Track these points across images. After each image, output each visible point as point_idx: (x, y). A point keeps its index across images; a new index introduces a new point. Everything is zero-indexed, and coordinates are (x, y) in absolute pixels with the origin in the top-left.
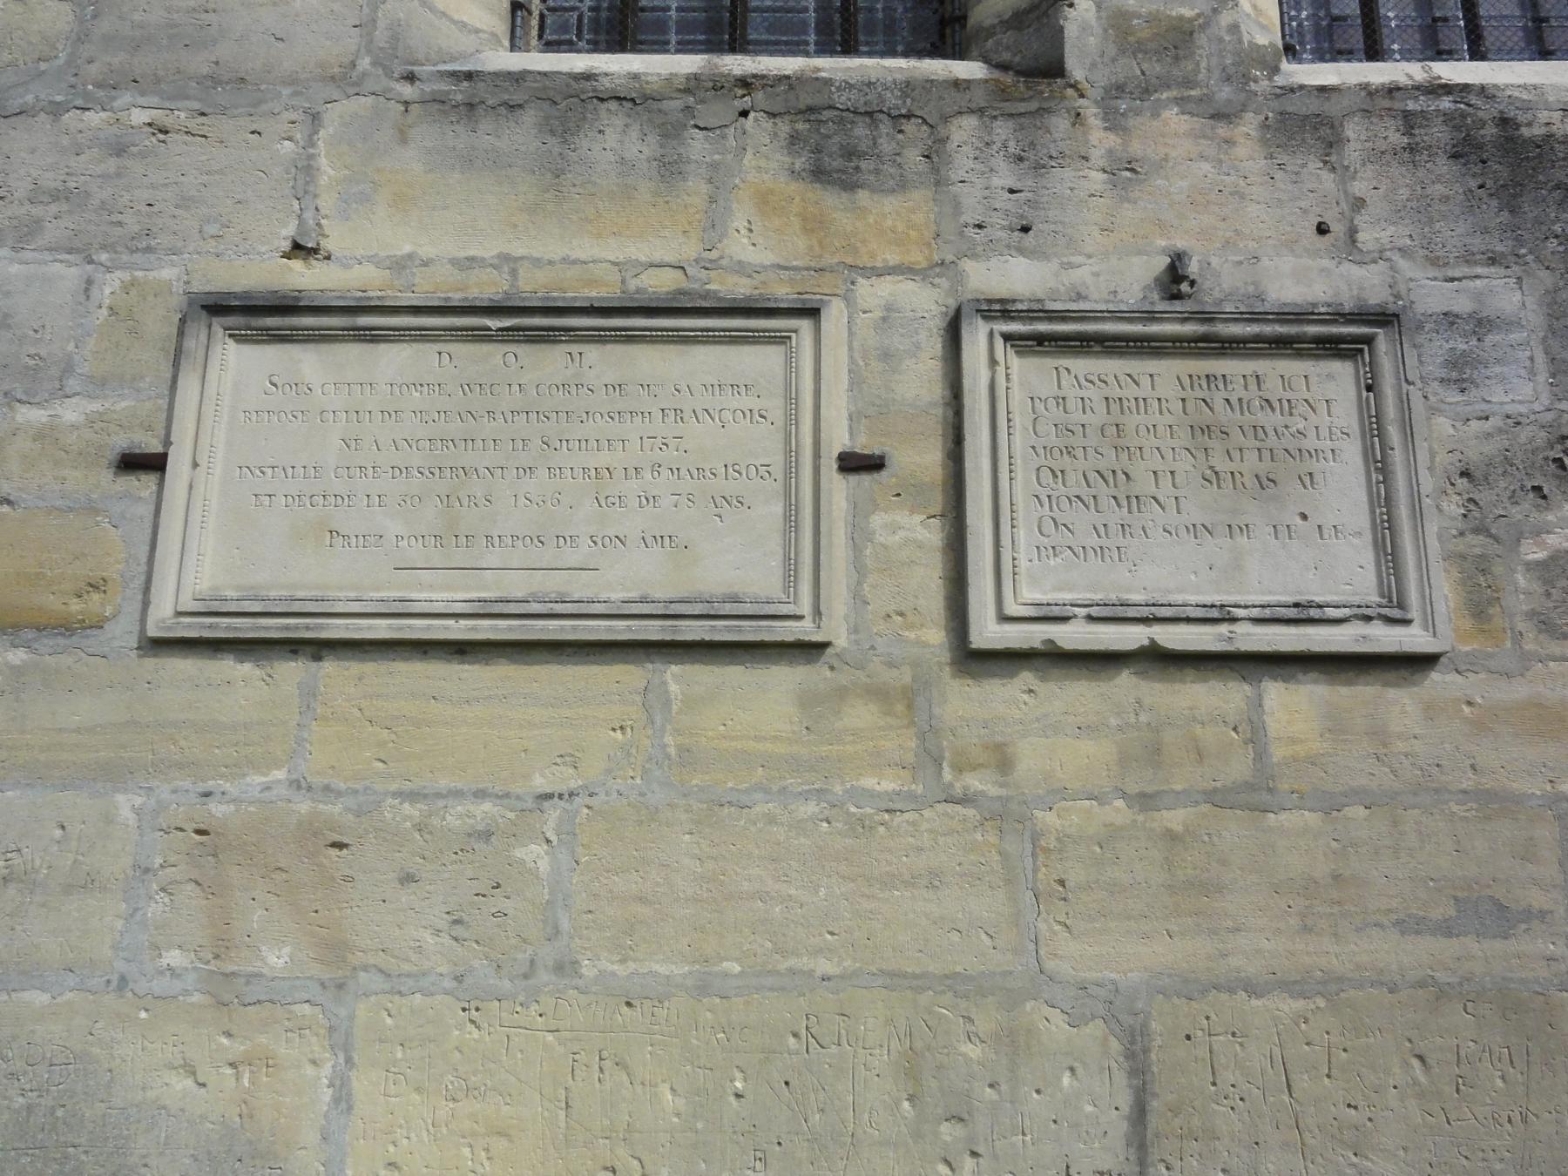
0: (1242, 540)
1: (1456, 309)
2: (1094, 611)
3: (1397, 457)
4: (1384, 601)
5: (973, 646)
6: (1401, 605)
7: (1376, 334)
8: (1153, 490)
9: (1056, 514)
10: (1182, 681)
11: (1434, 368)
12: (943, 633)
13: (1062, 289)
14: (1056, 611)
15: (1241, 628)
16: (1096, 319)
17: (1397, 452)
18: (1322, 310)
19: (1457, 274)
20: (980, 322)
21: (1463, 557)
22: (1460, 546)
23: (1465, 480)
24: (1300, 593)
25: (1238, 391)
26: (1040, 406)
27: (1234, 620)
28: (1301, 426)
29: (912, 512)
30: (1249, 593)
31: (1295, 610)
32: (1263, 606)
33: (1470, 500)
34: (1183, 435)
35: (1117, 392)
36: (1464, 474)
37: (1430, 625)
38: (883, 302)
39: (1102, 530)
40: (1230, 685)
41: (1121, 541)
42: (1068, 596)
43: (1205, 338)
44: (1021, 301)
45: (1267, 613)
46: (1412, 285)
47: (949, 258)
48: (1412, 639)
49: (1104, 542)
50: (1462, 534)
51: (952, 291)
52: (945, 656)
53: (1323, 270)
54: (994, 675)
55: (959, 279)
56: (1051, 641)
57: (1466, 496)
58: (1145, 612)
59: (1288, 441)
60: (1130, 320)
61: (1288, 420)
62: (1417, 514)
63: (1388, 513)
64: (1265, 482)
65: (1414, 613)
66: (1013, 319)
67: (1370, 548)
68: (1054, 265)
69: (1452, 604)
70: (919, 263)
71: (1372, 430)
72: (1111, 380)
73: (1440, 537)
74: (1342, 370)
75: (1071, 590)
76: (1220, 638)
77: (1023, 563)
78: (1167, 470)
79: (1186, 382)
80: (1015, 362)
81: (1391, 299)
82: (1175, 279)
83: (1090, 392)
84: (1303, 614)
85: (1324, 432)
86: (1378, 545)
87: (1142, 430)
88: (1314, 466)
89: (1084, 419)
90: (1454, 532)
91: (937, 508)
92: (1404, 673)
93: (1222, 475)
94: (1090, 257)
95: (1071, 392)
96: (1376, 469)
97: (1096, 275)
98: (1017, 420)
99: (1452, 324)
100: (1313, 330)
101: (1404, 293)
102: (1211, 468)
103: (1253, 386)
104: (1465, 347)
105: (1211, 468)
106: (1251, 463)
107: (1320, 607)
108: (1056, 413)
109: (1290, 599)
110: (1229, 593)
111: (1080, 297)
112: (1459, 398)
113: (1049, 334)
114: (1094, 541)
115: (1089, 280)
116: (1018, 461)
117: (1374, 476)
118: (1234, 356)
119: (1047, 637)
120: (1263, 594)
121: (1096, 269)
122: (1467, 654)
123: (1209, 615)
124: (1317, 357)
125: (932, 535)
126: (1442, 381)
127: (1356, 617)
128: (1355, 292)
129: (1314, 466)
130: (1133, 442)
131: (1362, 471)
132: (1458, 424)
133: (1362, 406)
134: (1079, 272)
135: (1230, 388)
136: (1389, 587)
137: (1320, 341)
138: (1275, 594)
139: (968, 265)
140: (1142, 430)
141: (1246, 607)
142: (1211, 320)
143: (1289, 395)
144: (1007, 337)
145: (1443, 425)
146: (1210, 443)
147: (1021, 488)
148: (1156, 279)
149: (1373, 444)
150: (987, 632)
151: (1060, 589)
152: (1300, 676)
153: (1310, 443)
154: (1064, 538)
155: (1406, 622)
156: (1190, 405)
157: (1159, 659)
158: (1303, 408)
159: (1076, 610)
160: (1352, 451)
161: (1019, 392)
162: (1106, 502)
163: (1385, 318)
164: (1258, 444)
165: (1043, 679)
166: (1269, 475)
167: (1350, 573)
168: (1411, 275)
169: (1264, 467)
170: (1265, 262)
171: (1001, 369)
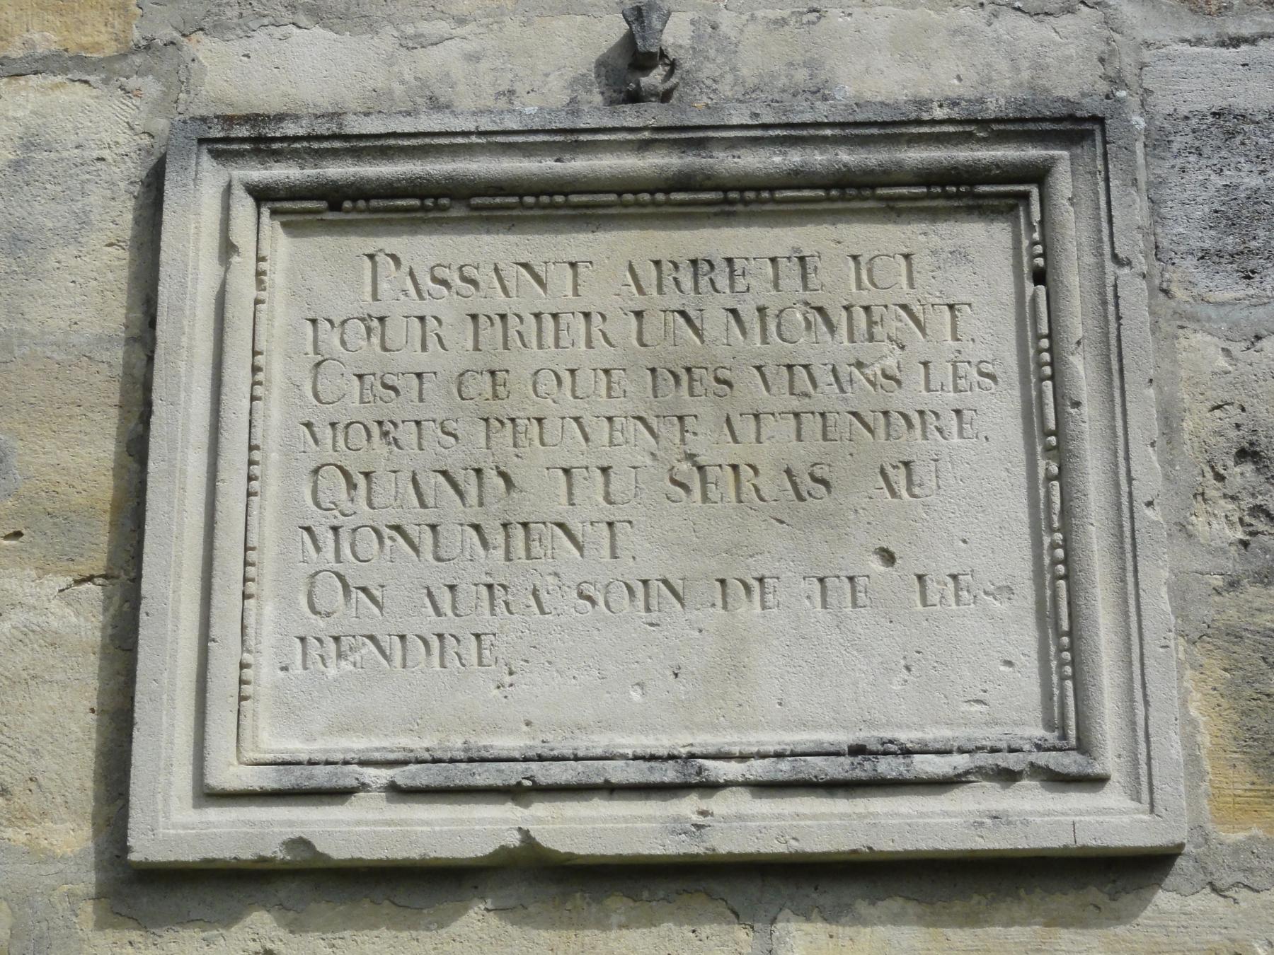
0: (748, 610)
1: (1241, 103)
2: (401, 776)
3: (1088, 421)
4: (1052, 737)
5: (134, 857)
6: (1083, 747)
7: (1053, 160)
8: (560, 508)
9: (350, 567)
10: (603, 925)
11: (1188, 227)
12: (87, 831)
13: (398, 89)
14: (321, 777)
15: (720, 804)
16: (455, 151)
17: (1086, 410)
18: (939, 114)
19: (1247, 29)
20: (207, 162)
21: (1235, 635)
22: (1231, 610)
23: (1248, 468)
24: (870, 724)
25: (758, 288)
26: (331, 339)
27: (710, 787)
28: (890, 363)
29: (43, 571)
30: (755, 727)
31: (846, 761)
32: (779, 755)
33: (1258, 510)
34: (636, 387)
35: (500, 302)
36: (1246, 454)
37: (1144, 787)
38: (20, 131)
39: (445, 599)
40: (705, 930)
41: (484, 620)
42: (358, 744)
43: (683, 182)
44: (296, 118)
45: (784, 769)
46: (1147, 55)
47: (165, 33)
48: (1105, 819)
49: (448, 624)
50: (1233, 584)
51: (167, 102)
52: (87, 881)
53: (956, 32)
54: (186, 921)
55: (182, 78)
56: (302, 843)
57: (1248, 502)
58: (512, 774)
59: (863, 397)
60: (527, 150)
61: (864, 350)
62: (1126, 545)
63: (1066, 545)
64: (806, 483)
65: (1110, 760)
66: (277, 155)
67: (1030, 620)
68: (386, 40)
69: (1205, 740)
70: (97, 46)
71: (1040, 365)
72: (485, 276)
73: (1179, 593)
74: (986, 244)
75: (366, 731)
76: (677, 827)
77: (265, 673)
78: (594, 462)
79: (649, 274)
80: (281, 246)
81: (1103, 87)
82: (633, 66)
83: (447, 307)
84: (864, 772)
85: (941, 372)
86: (1045, 616)
87: (547, 380)
88: (916, 445)
89: (421, 361)
90: (1218, 581)
91: (98, 563)
92: (1094, 894)
93: (712, 473)
94: (461, 21)
95: (397, 300)
96: (1048, 449)
97: (473, 58)
98: (276, 367)
99: (1231, 135)
100: (915, 156)
101: (1129, 75)
102: (691, 457)
103: (791, 278)
104: (1255, 181)
105: (691, 457)
106: (779, 444)
107: (907, 752)
108: (366, 350)
109: (844, 738)
110: (714, 728)
111: (436, 104)
112: (1241, 290)
113: (347, 186)
114: (427, 622)
115: (458, 70)
116: (272, 457)
117: (1042, 463)
118: (751, 218)
119: (296, 833)
120: (786, 727)
121: (468, 47)
122: (1236, 850)
123: (656, 778)
124: (934, 215)
125: (82, 619)
126: (1204, 255)
127: (984, 773)
128: (1025, 75)
129: (916, 445)
130: (521, 404)
131: (1021, 456)
132: (1236, 348)
133: (1024, 312)
134: (437, 53)
135: (741, 284)
136: (1063, 705)
137: (934, 178)
138: (817, 727)
139: (204, 49)
140: (547, 380)
141: (743, 758)
142: (699, 145)
143: (866, 297)
144: (261, 195)
145: (1203, 350)
146: (689, 405)
147: (272, 517)
148: (601, 63)
149: (1041, 394)
150: (171, 825)
151: (345, 729)
152: (862, 907)
153: (911, 396)
154: (353, 616)
155: (1096, 782)
156: (653, 325)
157: (537, 877)
158: (898, 324)
159: (370, 774)
160: (1000, 412)
161: (275, 301)
162: (459, 539)
163: (1076, 128)
164: (795, 404)
165: (295, 927)
166: (826, 466)
167: (985, 680)
168: (1148, 35)
169: (801, 455)
170: (836, 18)
171: (244, 264)
